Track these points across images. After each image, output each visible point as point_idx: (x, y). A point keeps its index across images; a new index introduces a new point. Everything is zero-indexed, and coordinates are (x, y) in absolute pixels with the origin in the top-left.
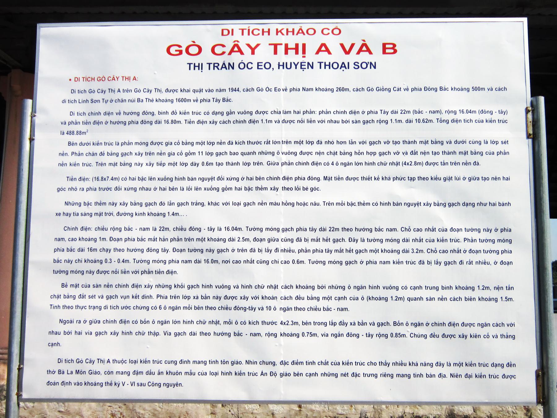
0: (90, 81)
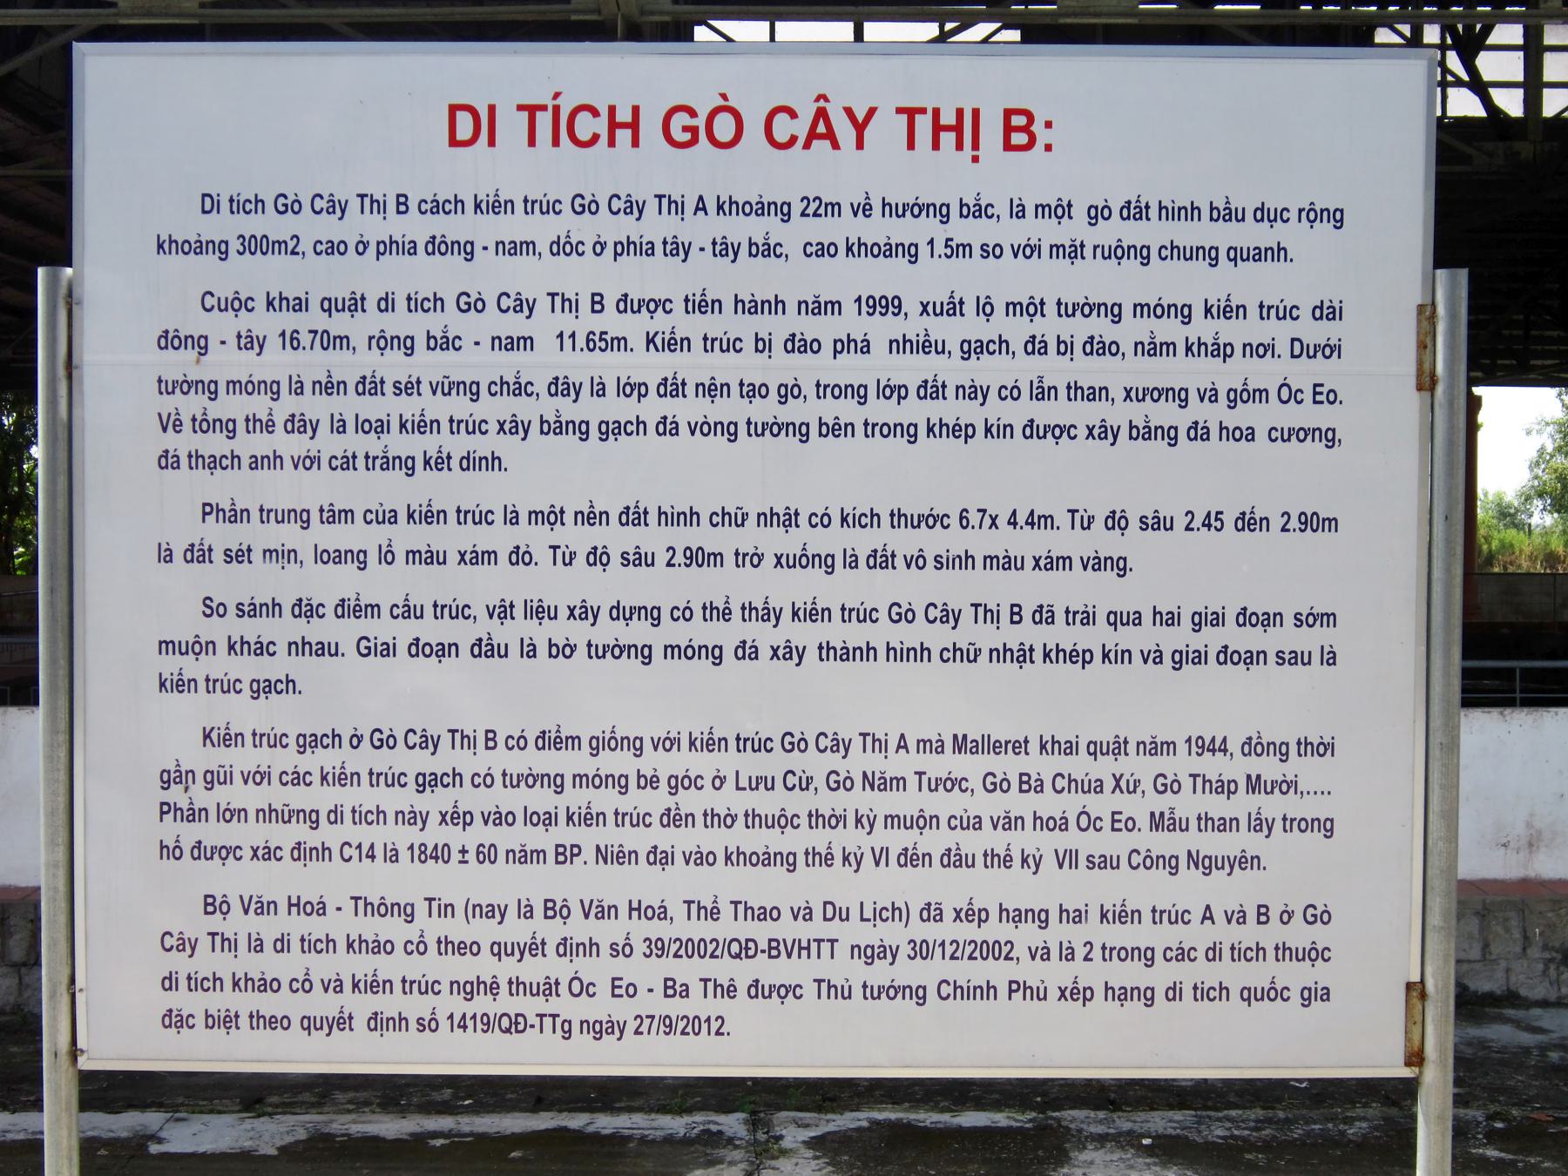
0: (595, 138)
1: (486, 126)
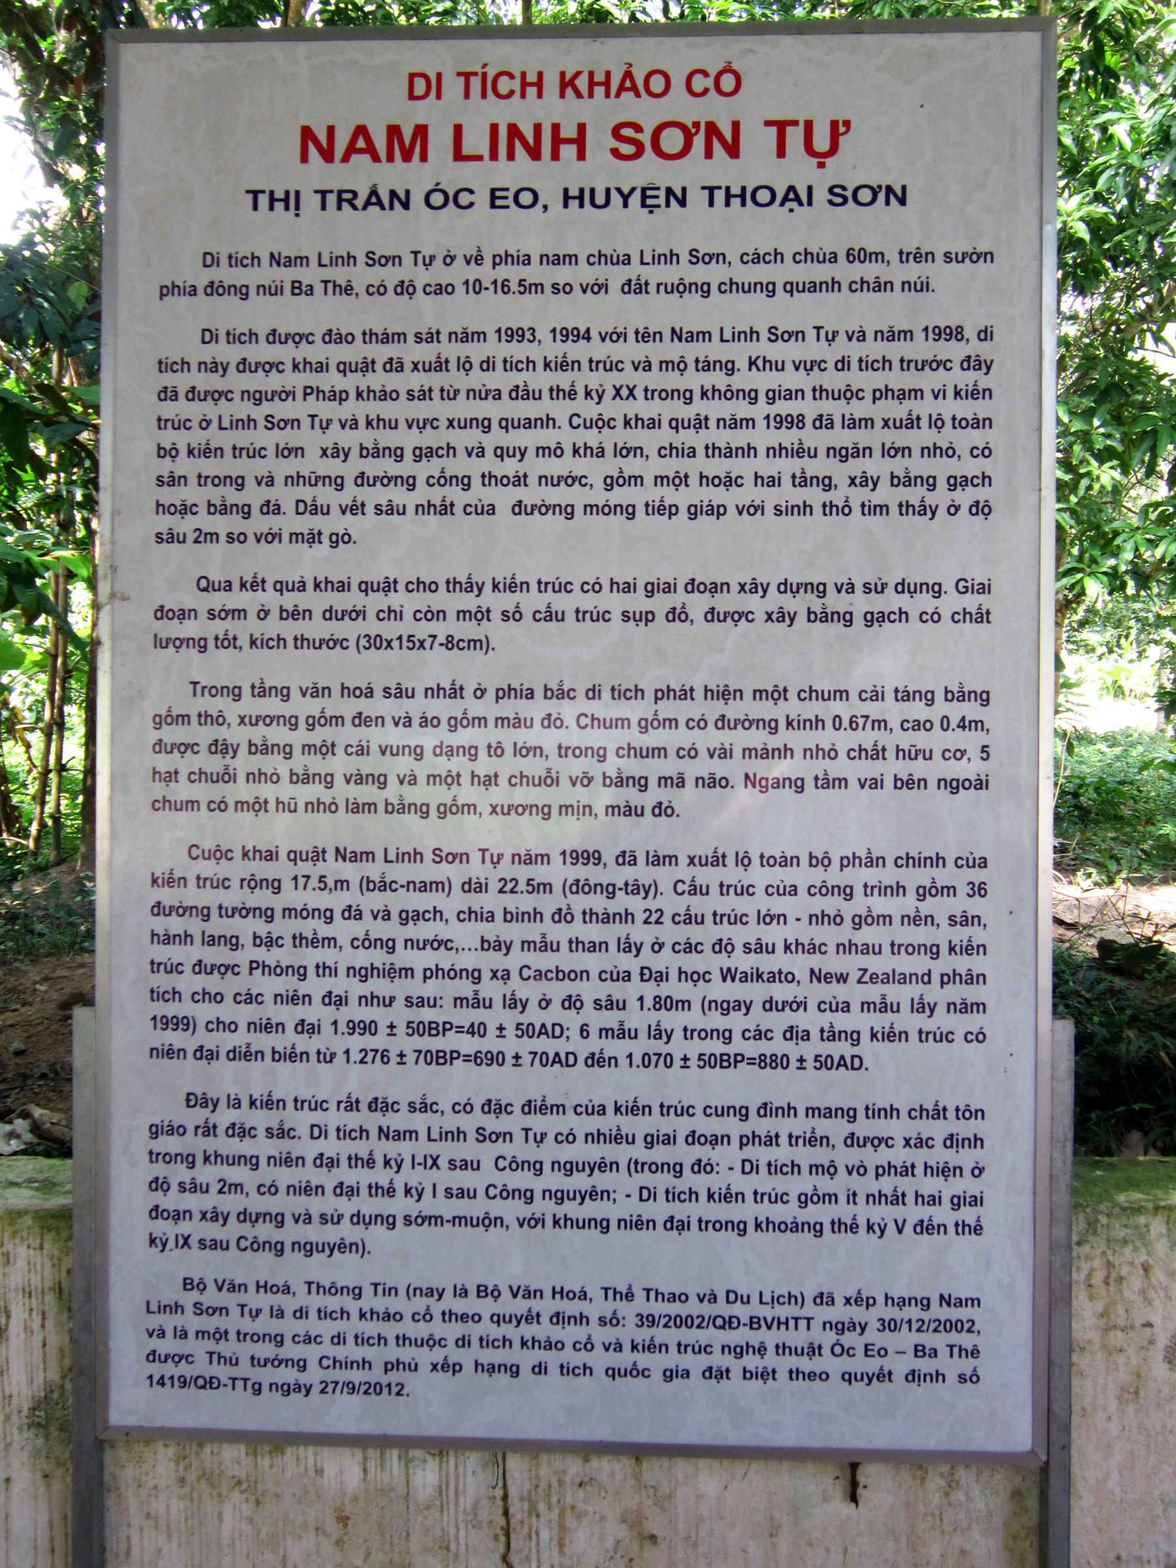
1: (436, 86)
